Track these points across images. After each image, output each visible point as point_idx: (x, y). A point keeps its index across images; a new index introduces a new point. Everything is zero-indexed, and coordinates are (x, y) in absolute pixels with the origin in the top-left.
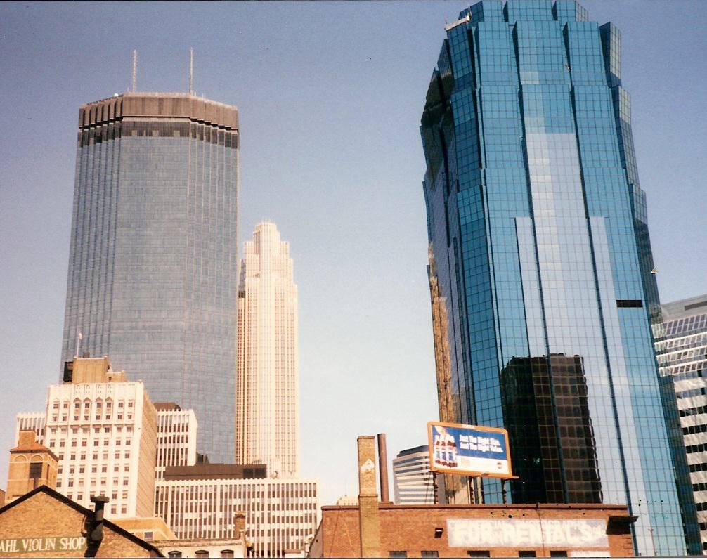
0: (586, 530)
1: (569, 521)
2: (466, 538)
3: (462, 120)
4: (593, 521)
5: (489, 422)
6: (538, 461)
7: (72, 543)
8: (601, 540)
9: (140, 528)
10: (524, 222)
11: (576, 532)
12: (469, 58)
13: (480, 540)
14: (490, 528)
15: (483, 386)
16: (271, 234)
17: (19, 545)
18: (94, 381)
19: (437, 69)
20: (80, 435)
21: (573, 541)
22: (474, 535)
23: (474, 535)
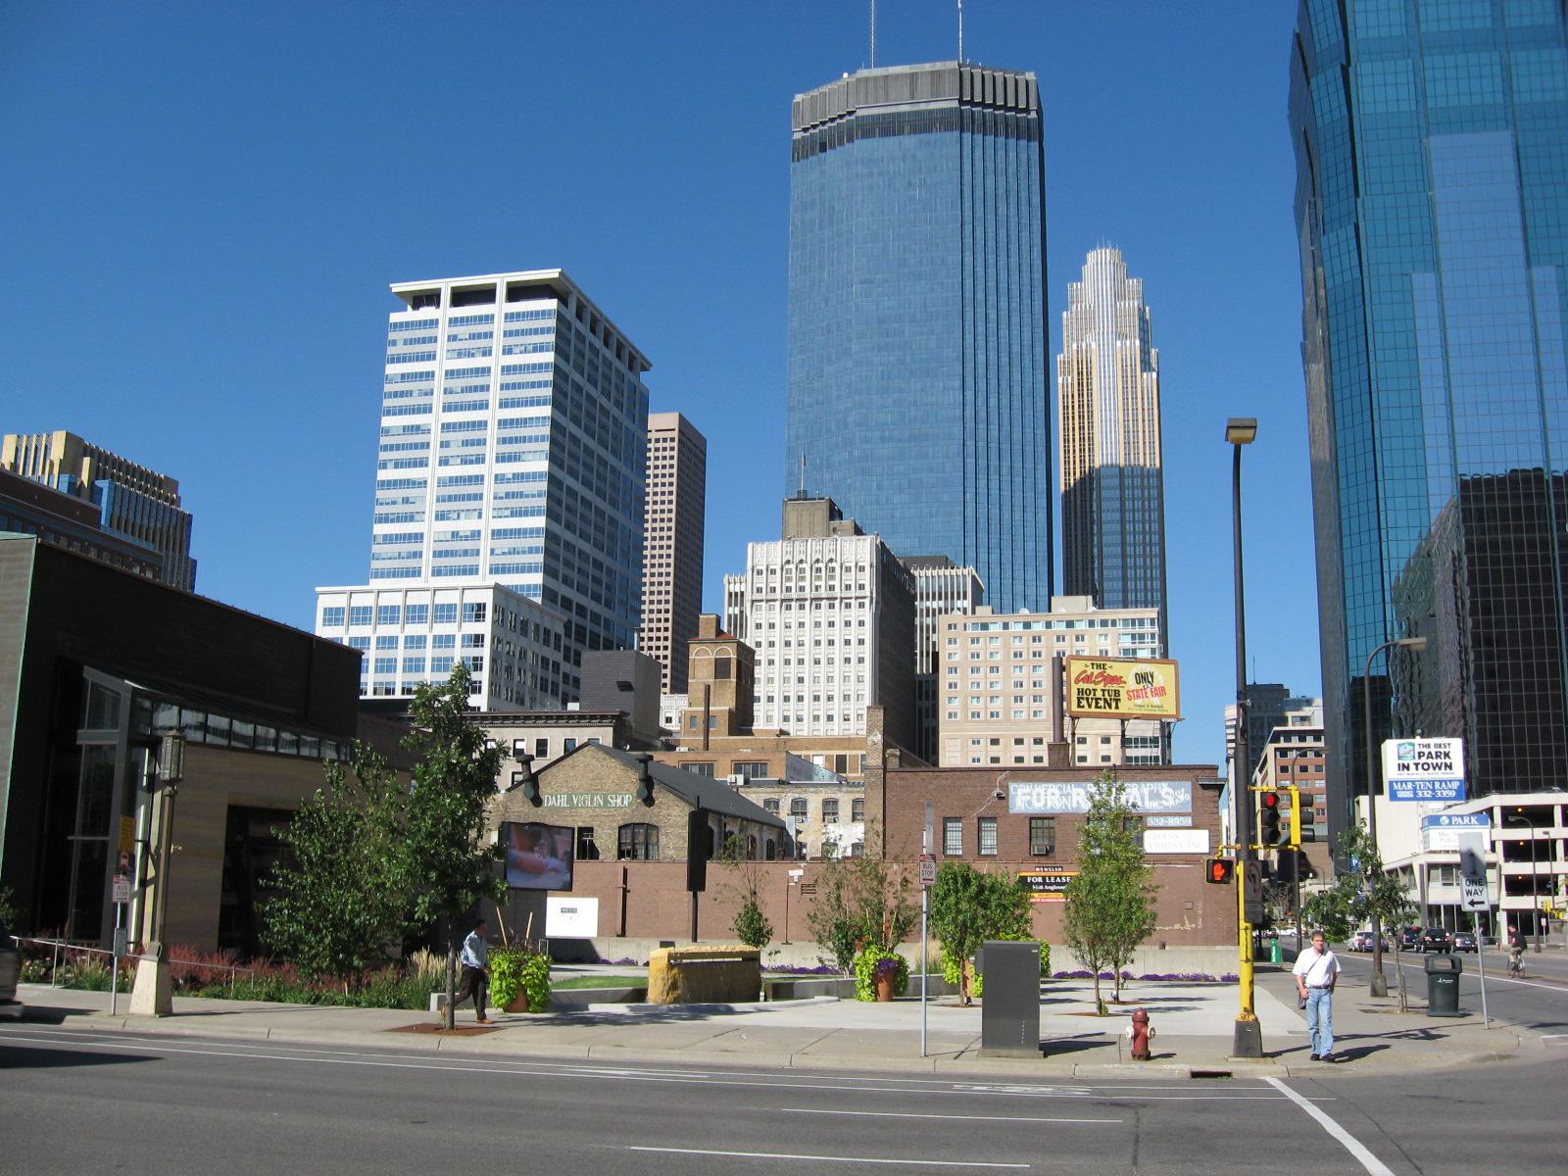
0: (1168, 793)
1: (1148, 784)
2: (1030, 803)
3: (1328, 119)
4: (1176, 783)
5: (151, 954)
6: (267, 908)
7: (619, 801)
8: (1183, 804)
9: (854, 749)
10: (1422, 281)
11: (1155, 796)
12: (1338, 17)
13: (1046, 805)
14: (1057, 792)
15: (1356, 540)
16: (1100, 266)
17: (570, 800)
18: (812, 534)
19: (1297, 31)
20: (794, 615)
21: (1151, 805)
22: (1039, 801)
23: (1039, 801)
